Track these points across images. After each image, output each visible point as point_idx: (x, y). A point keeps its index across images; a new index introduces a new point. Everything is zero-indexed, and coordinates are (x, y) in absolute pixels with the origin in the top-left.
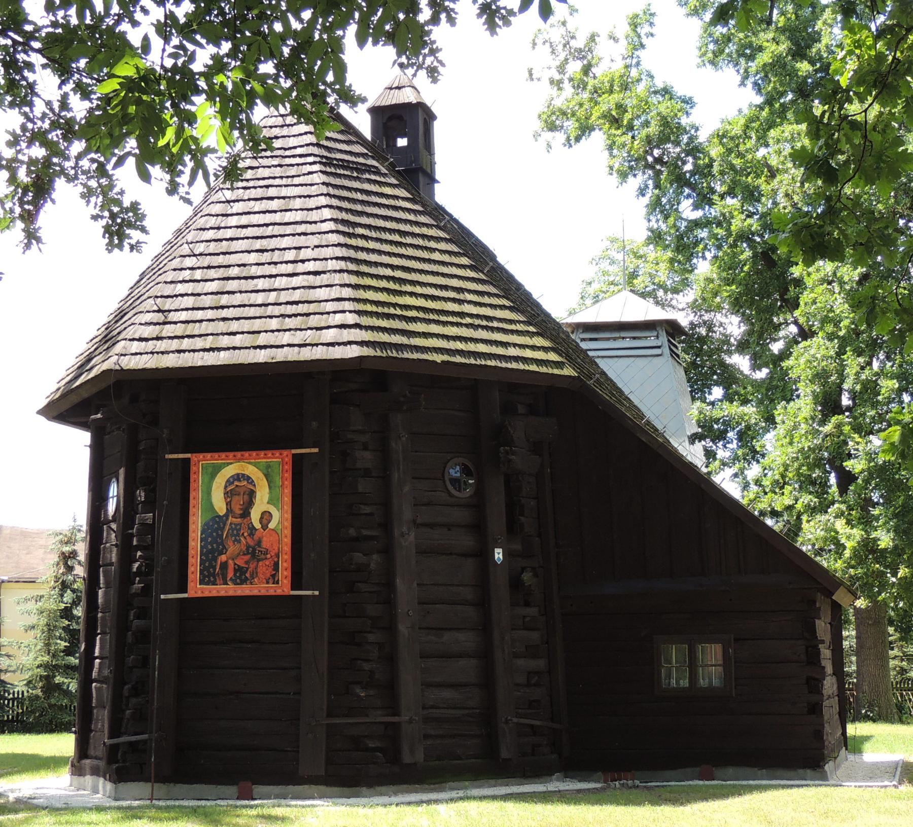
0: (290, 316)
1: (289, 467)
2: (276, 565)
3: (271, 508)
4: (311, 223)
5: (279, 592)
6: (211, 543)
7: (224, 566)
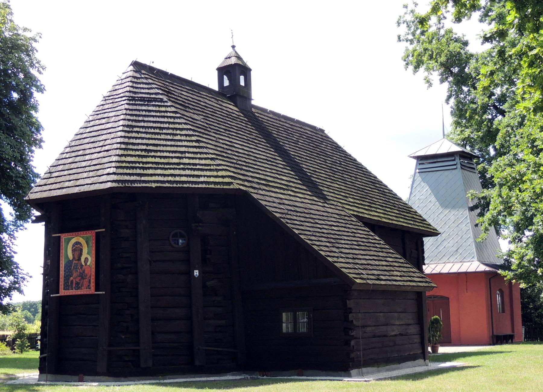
0: (92, 171)
1: (94, 238)
2: (90, 281)
3: (88, 257)
4: (114, 128)
5: (91, 293)
6: (67, 272)
7: (72, 281)
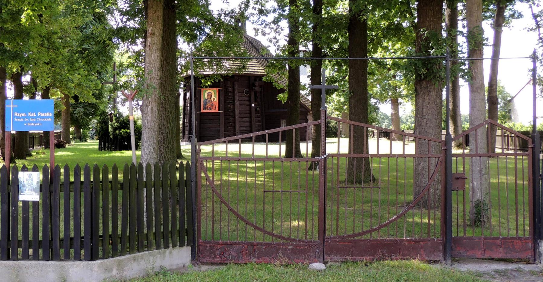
3: (215, 98)
